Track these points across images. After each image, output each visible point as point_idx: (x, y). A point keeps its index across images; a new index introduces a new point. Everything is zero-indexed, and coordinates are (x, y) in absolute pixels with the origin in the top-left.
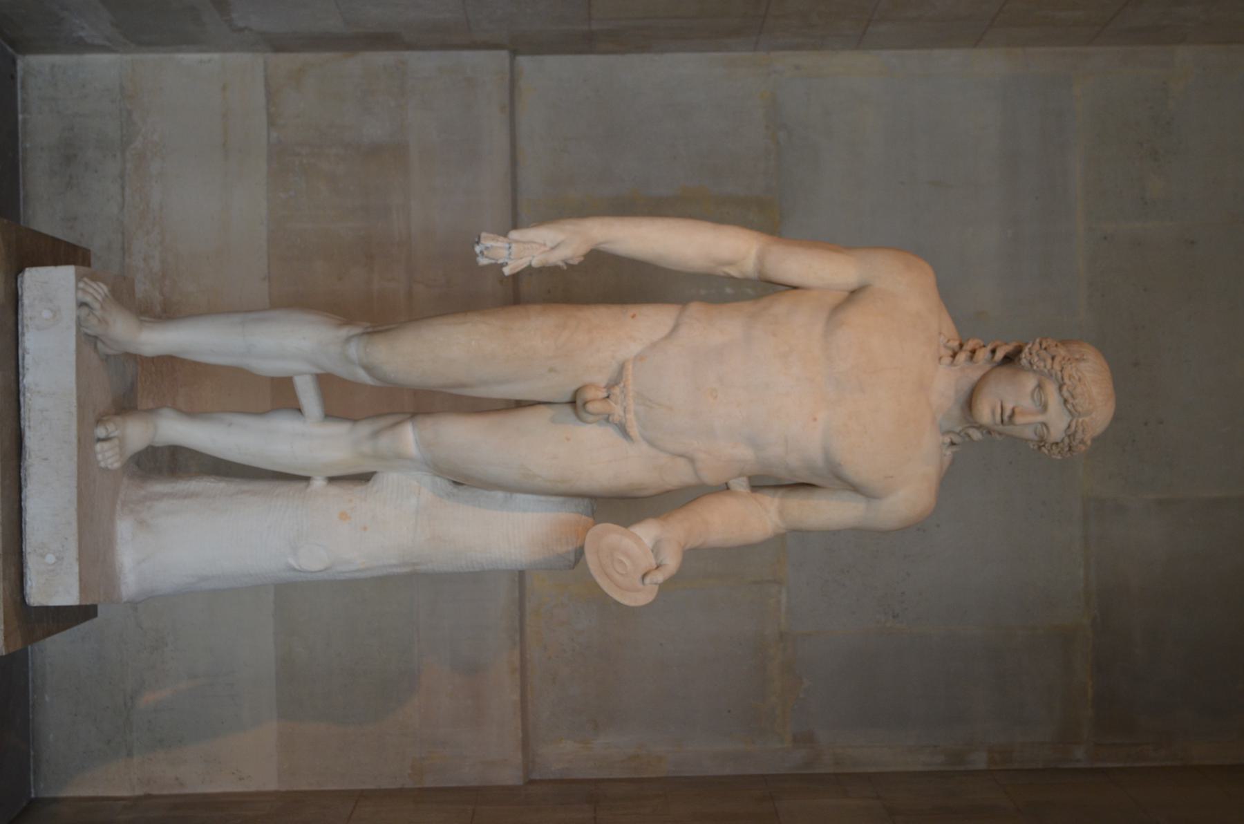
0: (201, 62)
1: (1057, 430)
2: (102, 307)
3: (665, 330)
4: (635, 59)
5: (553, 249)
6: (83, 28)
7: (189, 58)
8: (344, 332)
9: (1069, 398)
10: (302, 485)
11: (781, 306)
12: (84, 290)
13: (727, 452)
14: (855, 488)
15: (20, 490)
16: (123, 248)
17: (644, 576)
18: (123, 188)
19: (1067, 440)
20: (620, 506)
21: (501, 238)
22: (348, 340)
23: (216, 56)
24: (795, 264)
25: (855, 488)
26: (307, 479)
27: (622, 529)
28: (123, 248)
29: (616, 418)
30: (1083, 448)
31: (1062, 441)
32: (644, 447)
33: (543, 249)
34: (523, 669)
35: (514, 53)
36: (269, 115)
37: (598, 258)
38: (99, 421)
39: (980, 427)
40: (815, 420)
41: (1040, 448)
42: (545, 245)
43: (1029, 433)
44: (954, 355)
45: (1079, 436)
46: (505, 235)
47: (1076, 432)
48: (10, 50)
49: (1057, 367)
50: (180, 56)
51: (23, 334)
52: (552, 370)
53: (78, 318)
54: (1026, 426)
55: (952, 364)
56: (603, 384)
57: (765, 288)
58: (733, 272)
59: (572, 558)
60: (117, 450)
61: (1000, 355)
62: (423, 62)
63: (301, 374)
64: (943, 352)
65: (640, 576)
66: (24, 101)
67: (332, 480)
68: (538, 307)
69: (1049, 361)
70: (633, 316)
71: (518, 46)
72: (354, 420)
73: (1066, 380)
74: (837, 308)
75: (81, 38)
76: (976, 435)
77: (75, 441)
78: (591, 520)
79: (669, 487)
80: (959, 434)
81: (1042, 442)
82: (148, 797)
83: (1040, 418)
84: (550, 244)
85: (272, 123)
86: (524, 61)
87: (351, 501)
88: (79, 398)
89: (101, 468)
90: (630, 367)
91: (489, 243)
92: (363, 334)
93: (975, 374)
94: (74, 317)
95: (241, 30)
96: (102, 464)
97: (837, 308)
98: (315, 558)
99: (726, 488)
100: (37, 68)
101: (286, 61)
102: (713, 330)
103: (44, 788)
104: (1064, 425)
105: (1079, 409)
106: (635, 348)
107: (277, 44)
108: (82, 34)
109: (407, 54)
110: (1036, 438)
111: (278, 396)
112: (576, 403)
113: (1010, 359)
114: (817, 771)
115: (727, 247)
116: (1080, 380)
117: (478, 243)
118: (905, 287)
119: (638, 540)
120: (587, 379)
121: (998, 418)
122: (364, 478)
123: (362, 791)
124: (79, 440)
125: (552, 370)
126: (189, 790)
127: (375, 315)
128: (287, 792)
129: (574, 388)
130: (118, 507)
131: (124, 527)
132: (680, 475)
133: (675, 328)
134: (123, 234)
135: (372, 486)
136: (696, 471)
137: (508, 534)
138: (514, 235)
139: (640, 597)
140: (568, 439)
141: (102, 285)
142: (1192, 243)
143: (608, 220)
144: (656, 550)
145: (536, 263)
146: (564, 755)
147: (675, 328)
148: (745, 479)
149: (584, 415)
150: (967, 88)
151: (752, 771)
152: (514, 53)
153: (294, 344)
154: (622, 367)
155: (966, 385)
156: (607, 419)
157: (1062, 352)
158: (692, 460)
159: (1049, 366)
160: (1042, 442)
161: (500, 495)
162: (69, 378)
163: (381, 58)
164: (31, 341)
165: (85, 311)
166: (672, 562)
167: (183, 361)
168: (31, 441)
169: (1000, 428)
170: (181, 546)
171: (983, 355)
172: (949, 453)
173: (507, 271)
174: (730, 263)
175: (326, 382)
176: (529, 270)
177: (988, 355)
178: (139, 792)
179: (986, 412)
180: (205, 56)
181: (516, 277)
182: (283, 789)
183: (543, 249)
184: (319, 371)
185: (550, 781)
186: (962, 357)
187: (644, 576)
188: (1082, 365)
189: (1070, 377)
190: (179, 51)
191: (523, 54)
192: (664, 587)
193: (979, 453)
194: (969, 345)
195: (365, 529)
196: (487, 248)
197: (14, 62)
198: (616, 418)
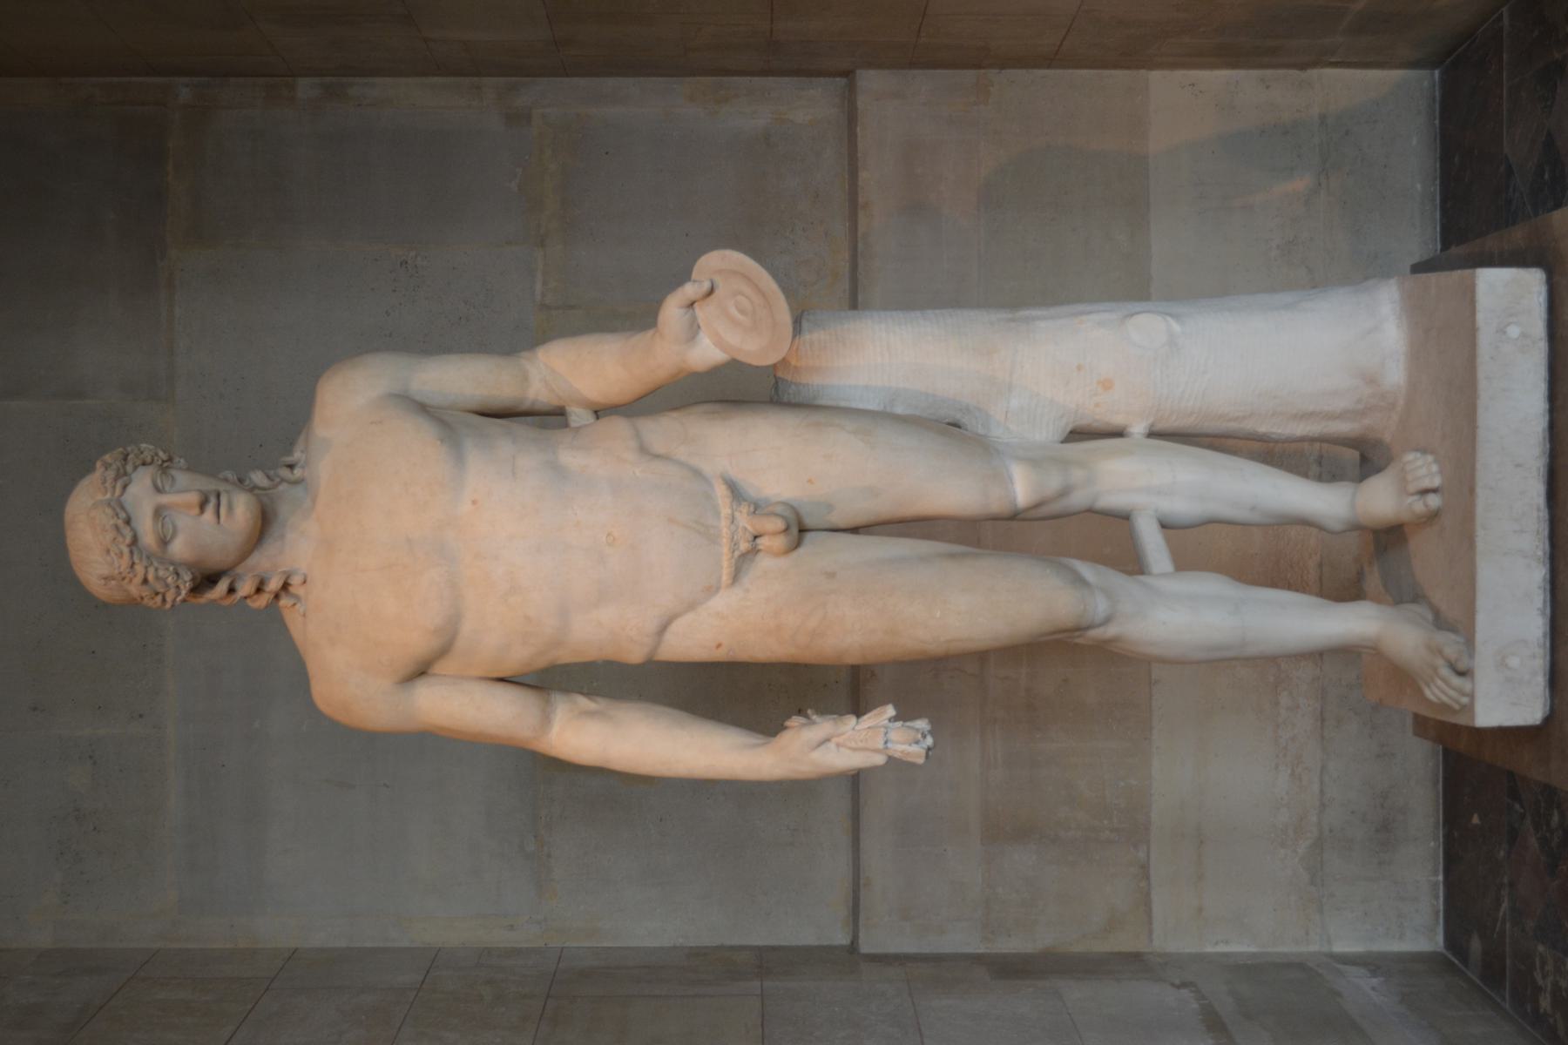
0: (1227, 942)
2: (1435, 669)
3: (677, 626)
4: (707, 940)
5: (828, 740)
6: (1373, 989)
7: (1241, 947)
8: (1111, 631)
9: (124, 526)
10: (1160, 426)
11: (519, 657)
14: (423, 409)
16: (1323, 720)
17: (711, 292)
18: (1322, 792)
19: (129, 468)
21: (897, 755)
22: (1107, 620)
23: (1209, 949)
24: (500, 714)
25: (423, 409)
26: (1153, 434)
28: (1323, 720)
29: (744, 509)
30: (107, 457)
31: (135, 468)
32: (707, 469)
33: (840, 740)
34: (854, 205)
35: (853, 948)
36: (1148, 877)
38: (1433, 516)
39: (253, 489)
40: (474, 502)
41: (170, 459)
42: (838, 745)
43: (182, 478)
44: (286, 586)
45: (111, 474)
46: (891, 759)
47: (115, 480)
49: (139, 569)
50: (1253, 949)
53: (1471, 656)
54: (184, 492)
56: (760, 555)
58: (583, 702)
59: (805, 324)
60: (1409, 477)
61: (223, 586)
62: (961, 940)
63: (1164, 575)
64: (301, 591)
65: (717, 292)
66: (1437, 898)
67: (1118, 433)
69: (150, 577)
70: (719, 646)
71: (849, 958)
72: (1091, 511)
73: (126, 550)
74: (444, 652)
75: (1374, 973)
76: (258, 478)
77: (1479, 491)
78: (780, 374)
79: (675, 414)
80: (283, 480)
82: (1303, 67)
84: (832, 745)
86: (841, 938)
87: (1097, 405)
89: (1432, 453)
90: (725, 578)
91: (914, 749)
92: (1089, 627)
93: (260, 561)
95: (1184, 985)
96: (1430, 458)
97: (444, 652)
98: (1148, 328)
99: (600, 412)
100: (1419, 932)
101: (1124, 942)
102: (613, 627)
104: (133, 489)
105: (109, 511)
106: (719, 602)
107: (1136, 964)
108: (1375, 981)
110: (173, 472)
111: (1204, 545)
112: (799, 530)
113: (206, 579)
114: (502, 80)
115: (588, 735)
116: (108, 551)
117: (929, 749)
118: (351, 678)
119: (720, 343)
120: (784, 562)
121: (224, 500)
122: (1078, 434)
123: (1049, 67)
125: (831, 575)
126: (1255, 73)
127: (1063, 649)
128: (1138, 67)
129: (801, 550)
130: (1401, 402)
131: (1395, 375)
132: (662, 431)
133: (663, 629)
134: (1323, 737)
135: (1067, 424)
137: (885, 355)
139: (718, 263)
140: (810, 481)
141: (1432, 697)
142: (35, 709)
144: (693, 329)
146: (806, 105)
147: (663, 629)
148: (573, 424)
149: (787, 513)
150: (308, 897)
151: (582, 82)
152: (853, 948)
153: (1179, 614)
154: (736, 577)
156: (757, 508)
157: (134, 589)
158: (644, 450)
160: (165, 468)
161: (899, 410)
163: (1012, 945)
165: (1461, 666)
166: (672, 310)
167: (1322, 594)
168: (1536, 490)
169: (222, 487)
170: (1330, 346)
171: (246, 587)
172: (297, 455)
173: (890, 711)
174: (590, 714)
175: (1131, 562)
177: (238, 586)
178: (1314, 73)
179: (241, 509)
182: (1143, 72)
183: (840, 740)
184: (1141, 578)
185: (820, 73)
186: (274, 584)
187: (711, 292)
188: (105, 571)
189: (121, 555)
190: (1254, 955)
191: (841, 947)
192: (684, 277)
193: (260, 450)
194: (262, 601)
195: (1079, 368)
196: (917, 742)
198: (744, 509)
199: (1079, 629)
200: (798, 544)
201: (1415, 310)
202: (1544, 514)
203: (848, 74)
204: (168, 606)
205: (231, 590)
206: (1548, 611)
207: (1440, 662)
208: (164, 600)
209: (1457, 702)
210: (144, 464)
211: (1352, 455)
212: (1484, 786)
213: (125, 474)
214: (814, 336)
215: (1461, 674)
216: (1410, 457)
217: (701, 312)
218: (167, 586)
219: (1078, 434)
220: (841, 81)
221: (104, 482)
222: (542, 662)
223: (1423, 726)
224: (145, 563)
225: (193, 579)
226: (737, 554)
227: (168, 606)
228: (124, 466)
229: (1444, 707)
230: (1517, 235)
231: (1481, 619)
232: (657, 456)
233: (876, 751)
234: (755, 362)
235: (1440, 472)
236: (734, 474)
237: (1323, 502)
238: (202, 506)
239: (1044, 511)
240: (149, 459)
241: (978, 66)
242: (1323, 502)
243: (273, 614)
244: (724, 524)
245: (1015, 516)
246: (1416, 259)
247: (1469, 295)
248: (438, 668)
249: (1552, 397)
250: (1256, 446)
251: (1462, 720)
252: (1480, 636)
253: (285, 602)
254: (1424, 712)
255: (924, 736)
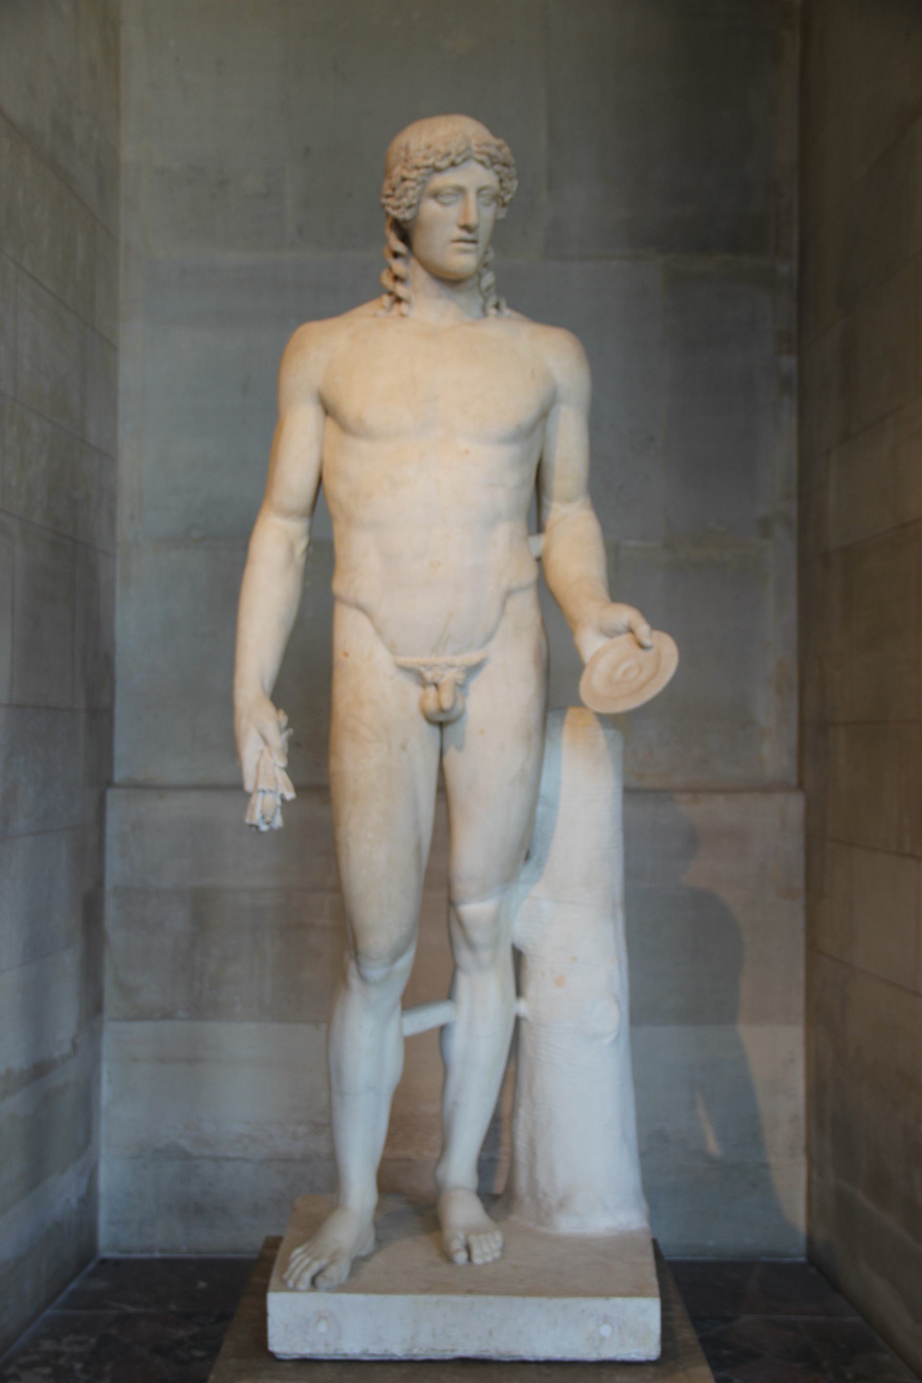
1: (491, 162)
2: (317, 1258)
3: (362, 619)
4: (121, 668)
7: (106, 1092)
8: (354, 982)
10: (524, 1027)
11: (338, 489)
12: (296, 1282)
13: (501, 555)
14: (545, 414)
15: (524, 1363)
17: (642, 646)
18: (228, 1159)
19: (498, 167)
20: (558, 681)
21: (253, 800)
22: (363, 978)
24: (294, 474)
25: (545, 414)
26: (518, 1021)
27: (586, 673)
29: (460, 676)
30: (506, 150)
31: (498, 173)
34: (695, 791)
37: (279, 696)
38: (447, 1257)
39: (479, 275)
40: (467, 452)
42: (262, 752)
44: (399, 300)
45: (493, 151)
48: (91, 1266)
49: (414, 174)
51: (345, 1355)
52: (404, 747)
53: (329, 1290)
54: (483, 215)
55: (408, 302)
57: (319, 509)
58: (301, 545)
61: (400, 247)
62: (116, 870)
63: (401, 1027)
65: (640, 652)
67: (519, 992)
68: (333, 762)
69: (408, 184)
70: (346, 654)
71: (101, 778)
73: (430, 162)
77: (470, 1298)
79: (538, 621)
81: (496, 197)
82: (808, 1150)
83: (472, 196)
84: (261, 746)
85: (168, 1016)
86: (119, 775)
88: (424, 1291)
90: (402, 660)
92: (358, 963)
93: (420, 277)
94: (327, 1295)
95: (75, 1046)
96: (497, 1255)
103: (797, 1252)
104: (480, 169)
105: (462, 147)
106: (382, 656)
107: (93, 1009)
109: (109, 885)
110: (493, 206)
111: (426, 1059)
112: (442, 722)
113: (404, 232)
117: (257, 827)
118: (323, 353)
119: (598, 655)
120: (415, 709)
122: (518, 957)
124: (470, 1292)
125: (404, 747)
129: (424, 725)
130: (544, 1230)
132: (525, 608)
136: (521, 589)
137: (586, 795)
138: (249, 786)
139: (667, 652)
143: (238, 682)
144: (610, 633)
145: (282, 762)
146: (775, 754)
152: (109, 783)
153: (370, 1041)
155: (431, 287)
156: (461, 687)
157: (398, 171)
158: (510, 593)
159: (413, 184)
160: (496, 197)
161: (540, 809)
162: (397, 1303)
163: (111, 911)
164: (354, 1344)
165: (320, 1281)
166: (626, 615)
168: (469, 1348)
169: (482, 245)
170: (593, 1168)
172: (507, 312)
173: (290, 795)
174: (291, 548)
176: (290, 770)
178: (802, 1158)
179: (463, 261)
180: (105, 1077)
181: (298, 789)
186: (401, 290)
187: (642, 646)
188: (413, 147)
189: (426, 158)
192: (655, 625)
193: (514, 280)
195: (574, 959)
196: (263, 817)
197: (104, 1262)
198: (460, 676)
199: (356, 954)
200: (430, 720)
201: (620, 1243)
202: (449, 1355)
203: (801, 786)
204: (384, 200)
205: (396, 255)
206: (366, 1358)
207: (324, 1262)
208: (388, 196)
209: (290, 1277)
210: (501, 181)
211: (499, 1186)
212: (231, 1290)
213: (493, 164)
214: (601, 737)
215: (313, 1281)
216: (498, 1236)
217: (625, 640)
218: (400, 198)
219: (518, 957)
220: (794, 780)
221: (487, 145)
222: (334, 508)
223: (273, 1244)
224: (420, 179)
225: (405, 221)
226: (423, 669)
227: (384, 200)
228: (499, 163)
229: (286, 1264)
230: (687, 1334)
231: (359, 1298)
232: (504, 604)
233: (256, 783)
234: (583, 684)
235: (486, 1264)
236: (488, 669)
237: (460, 1166)
238: (466, 228)
239: (455, 929)
240: (505, 185)
241: (808, 888)
242: (460, 1166)
243: (374, 292)
244: (446, 658)
245: (451, 904)
246: (661, 1241)
247: (637, 1292)
248: (330, 422)
249: (549, 1363)
250: (506, 1110)
251: (274, 1281)
252: (345, 1297)
253: (386, 300)
254: (283, 1247)
255: (268, 823)
